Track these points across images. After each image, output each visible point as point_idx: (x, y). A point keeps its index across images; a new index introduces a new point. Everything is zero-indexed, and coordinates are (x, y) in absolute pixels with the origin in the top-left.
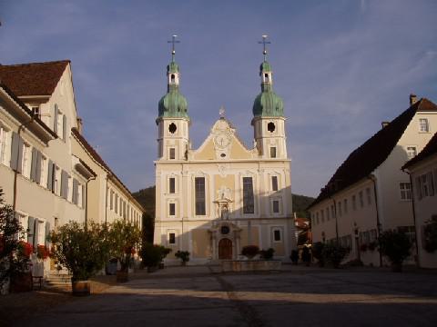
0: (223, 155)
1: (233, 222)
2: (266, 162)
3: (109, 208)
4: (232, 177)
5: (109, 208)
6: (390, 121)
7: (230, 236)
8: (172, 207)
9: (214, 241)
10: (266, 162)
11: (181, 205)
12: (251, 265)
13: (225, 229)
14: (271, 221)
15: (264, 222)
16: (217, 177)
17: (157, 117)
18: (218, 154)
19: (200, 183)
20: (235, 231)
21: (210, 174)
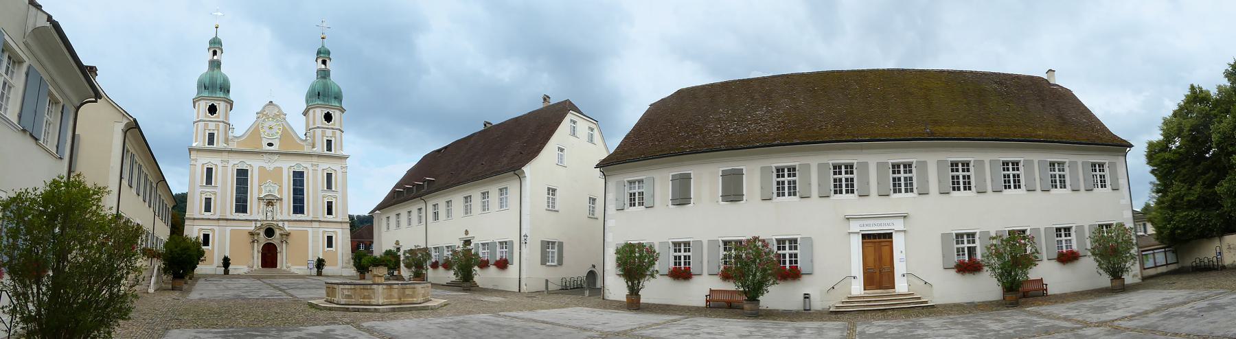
0: (270, 145)
1: (280, 224)
2: (320, 156)
3: (125, 183)
4: (279, 170)
5: (125, 183)
6: (494, 123)
7: (275, 240)
8: (208, 201)
9: (256, 244)
10: (320, 156)
11: (219, 202)
12: (395, 293)
13: (1101, 255)
14: (323, 225)
15: (316, 225)
16: (261, 169)
17: (224, 58)
18: (265, 143)
19: (242, 175)
20: (281, 235)
21: (254, 165)
